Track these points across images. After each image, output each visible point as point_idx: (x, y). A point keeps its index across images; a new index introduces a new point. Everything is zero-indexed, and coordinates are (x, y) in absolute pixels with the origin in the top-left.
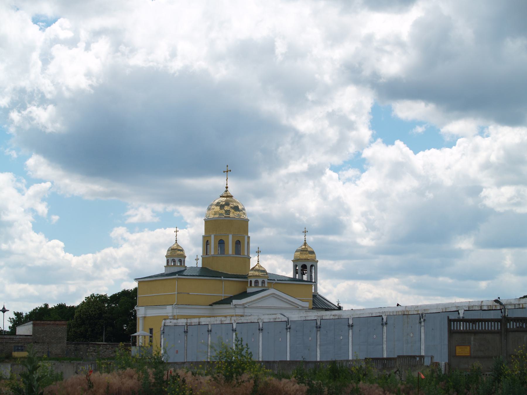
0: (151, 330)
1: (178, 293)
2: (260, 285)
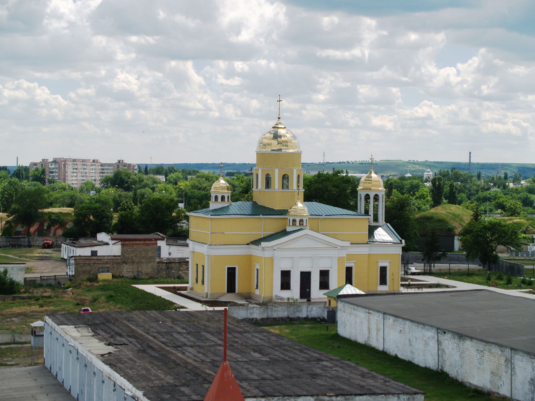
0: (197, 265)
1: (211, 233)
2: (298, 224)
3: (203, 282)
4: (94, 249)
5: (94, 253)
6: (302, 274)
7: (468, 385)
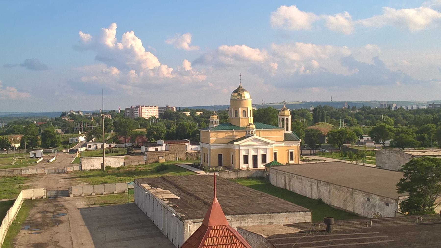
3: (207, 162)
4: (157, 148)
5: (156, 150)
6: (254, 156)
7: (332, 206)
